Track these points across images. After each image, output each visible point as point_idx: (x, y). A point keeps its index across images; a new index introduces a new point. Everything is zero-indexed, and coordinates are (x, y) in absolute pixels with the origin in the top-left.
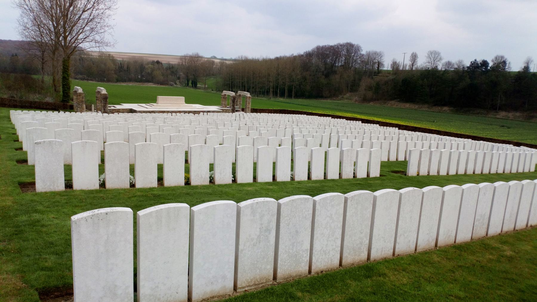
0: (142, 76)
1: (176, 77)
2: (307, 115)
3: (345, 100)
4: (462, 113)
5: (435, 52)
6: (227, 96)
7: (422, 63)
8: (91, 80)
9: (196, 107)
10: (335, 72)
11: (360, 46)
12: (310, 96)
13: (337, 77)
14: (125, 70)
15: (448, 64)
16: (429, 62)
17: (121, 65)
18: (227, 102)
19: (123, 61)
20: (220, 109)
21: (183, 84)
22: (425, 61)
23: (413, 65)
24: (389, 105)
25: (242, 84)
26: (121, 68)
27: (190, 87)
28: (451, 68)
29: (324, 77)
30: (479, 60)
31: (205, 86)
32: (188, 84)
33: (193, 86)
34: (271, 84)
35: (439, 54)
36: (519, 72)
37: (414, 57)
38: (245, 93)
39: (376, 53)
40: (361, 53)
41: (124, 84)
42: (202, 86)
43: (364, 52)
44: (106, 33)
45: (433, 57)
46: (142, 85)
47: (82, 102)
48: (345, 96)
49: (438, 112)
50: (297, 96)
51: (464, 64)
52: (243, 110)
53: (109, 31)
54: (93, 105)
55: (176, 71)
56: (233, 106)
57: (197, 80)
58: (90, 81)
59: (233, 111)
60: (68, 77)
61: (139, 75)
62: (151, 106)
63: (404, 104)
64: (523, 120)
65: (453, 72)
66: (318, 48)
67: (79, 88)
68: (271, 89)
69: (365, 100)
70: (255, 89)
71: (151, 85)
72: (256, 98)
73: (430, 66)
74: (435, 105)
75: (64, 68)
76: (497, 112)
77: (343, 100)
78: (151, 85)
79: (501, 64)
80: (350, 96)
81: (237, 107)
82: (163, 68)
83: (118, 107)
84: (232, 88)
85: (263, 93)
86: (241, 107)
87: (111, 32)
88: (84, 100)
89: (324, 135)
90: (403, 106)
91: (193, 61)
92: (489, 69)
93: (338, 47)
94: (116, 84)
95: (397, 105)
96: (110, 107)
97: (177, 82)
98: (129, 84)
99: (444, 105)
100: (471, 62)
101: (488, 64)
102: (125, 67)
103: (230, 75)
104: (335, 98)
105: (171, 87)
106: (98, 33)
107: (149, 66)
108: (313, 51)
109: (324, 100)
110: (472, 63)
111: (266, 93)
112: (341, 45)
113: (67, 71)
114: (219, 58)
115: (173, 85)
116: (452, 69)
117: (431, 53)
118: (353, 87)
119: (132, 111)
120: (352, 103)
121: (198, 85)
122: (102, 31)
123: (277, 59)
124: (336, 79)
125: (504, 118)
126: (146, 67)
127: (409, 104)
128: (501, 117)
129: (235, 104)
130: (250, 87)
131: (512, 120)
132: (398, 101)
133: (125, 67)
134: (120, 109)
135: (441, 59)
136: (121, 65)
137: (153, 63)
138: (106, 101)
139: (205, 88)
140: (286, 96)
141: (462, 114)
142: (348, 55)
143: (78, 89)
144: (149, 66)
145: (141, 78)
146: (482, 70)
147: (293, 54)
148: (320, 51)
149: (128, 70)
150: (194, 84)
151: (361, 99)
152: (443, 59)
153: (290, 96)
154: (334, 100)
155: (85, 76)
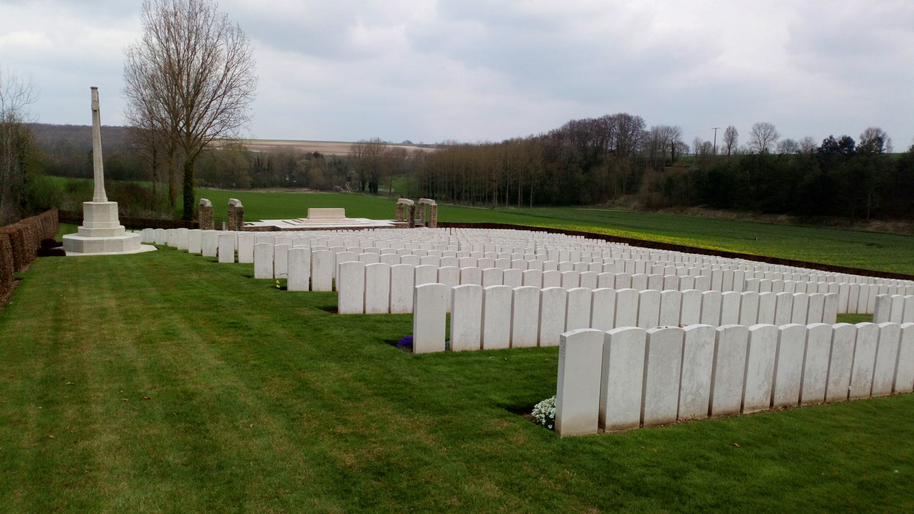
0: (292, 178)
1: (344, 177)
2: (517, 229)
3: (618, 208)
4: (808, 225)
5: (766, 125)
6: (404, 206)
7: (745, 143)
8: (212, 186)
9: (360, 222)
10: (599, 163)
11: (641, 119)
12: (559, 203)
13: (604, 169)
14: (265, 170)
15: (787, 144)
16: (756, 142)
17: (259, 161)
18: (403, 214)
19: (261, 153)
20: (394, 224)
21: (356, 188)
22: (750, 141)
23: (729, 148)
24: (690, 214)
25: (449, 187)
26: (259, 165)
27: (367, 193)
28: (793, 150)
29: (581, 170)
30: (838, 136)
31: (390, 189)
32: (363, 189)
33: (371, 192)
34: (495, 185)
35: (772, 128)
36: (904, 155)
37: (731, 135)
38: (429, 201)
39: (668, 130)
40: (643, 131)
41: (263, 191)
42: (386, 191)
43: (648, 129)
44: (241, 127)
45: (763, 133)
46: (292, 191)
47: (211, 218)
48: (617, 201)
49: (768, 224)
50: (538, 203)
51: (814, 144)
52: (427, 225)
53: (245, 124)
54: (224, 222)
55: (346, 167)
56: (412, 219)
57: (377, 182)
58: (211, 189)
59: (412, 225)
60: (191, 185)
61: (287, 175)
62: (300, 222)
63: (713, 212)
64: (909, 234)
65: (794, 157)
66: (572, 124)
67: (207, 200)
68: (494, 192)
69: (650, 206)
70: (470, 192)
71: (305, 191)
72: (472, 207)
73: (756, 150)
74: (765, 213)
75: (186, 174)
76: (867, 222)
77: (614, 207)
78: (305, 191)
79: (876, 140)
80: (625, 201)
81: (417, 221)
82: (325, 163)
83: (257, 224)
84: (433, 193)
85: (484, 200)
86: (425, 221)
87: (248, 126)
88: (212, 216)
89: (652, 277)
90: (711, 215)
91: (372, 151)
92: (854, 151)
93: (605, 121)
94: (251, 191)
95: (702, 214)
96: (246, 224)
97: (346, 185)
98: (271, 192)
99: (780, 212)
100: (825, 140)
101: (854, 143)
102: (265, 165)
103: (429, 171)
104: (600, 205)
105: (336, 193)
106: (230, 127)
107: (302, 161)
108: (564, 128)
109: (582, 208)
110: (827, 141)
111: (487, 199)
112: (610, 119)
113: (190, 179)
114: (415, 143)
115: (340, 190)
116: (794, 153)
117: (759, 127)
118: (630, 186)
119: (274, 229)
120: (628, 212)
121: (379, 190)
122: (237, 124)
123: (506, 143)
124: (601, 173)
125: (878, 231)
126: (298, 162)
127: (722, 212)
128: (875, 231)
129: (413, 216)
130: (462, 190)
131: (890, 234)
132: (705, 207)
133: (265, 165)
134: (259, 227)
135: (776, 136)
136: (259, 161)
137: (309, 156)
138: (242, 217)
139: (390, 194)
140: (519, 203)
141: (808, 227)
142: (622, 133)
143: (206, 202)
144: (302, 161)
145: (289, 180)
146: (843, 154)
147: (532, 135)
148: (576, 130)
149: (270, 167)
150: (374, 188)
151: (643, 204)
152: (780, 136)
153: (526, 203)
154: (599, 207)
155: (203, 180)
